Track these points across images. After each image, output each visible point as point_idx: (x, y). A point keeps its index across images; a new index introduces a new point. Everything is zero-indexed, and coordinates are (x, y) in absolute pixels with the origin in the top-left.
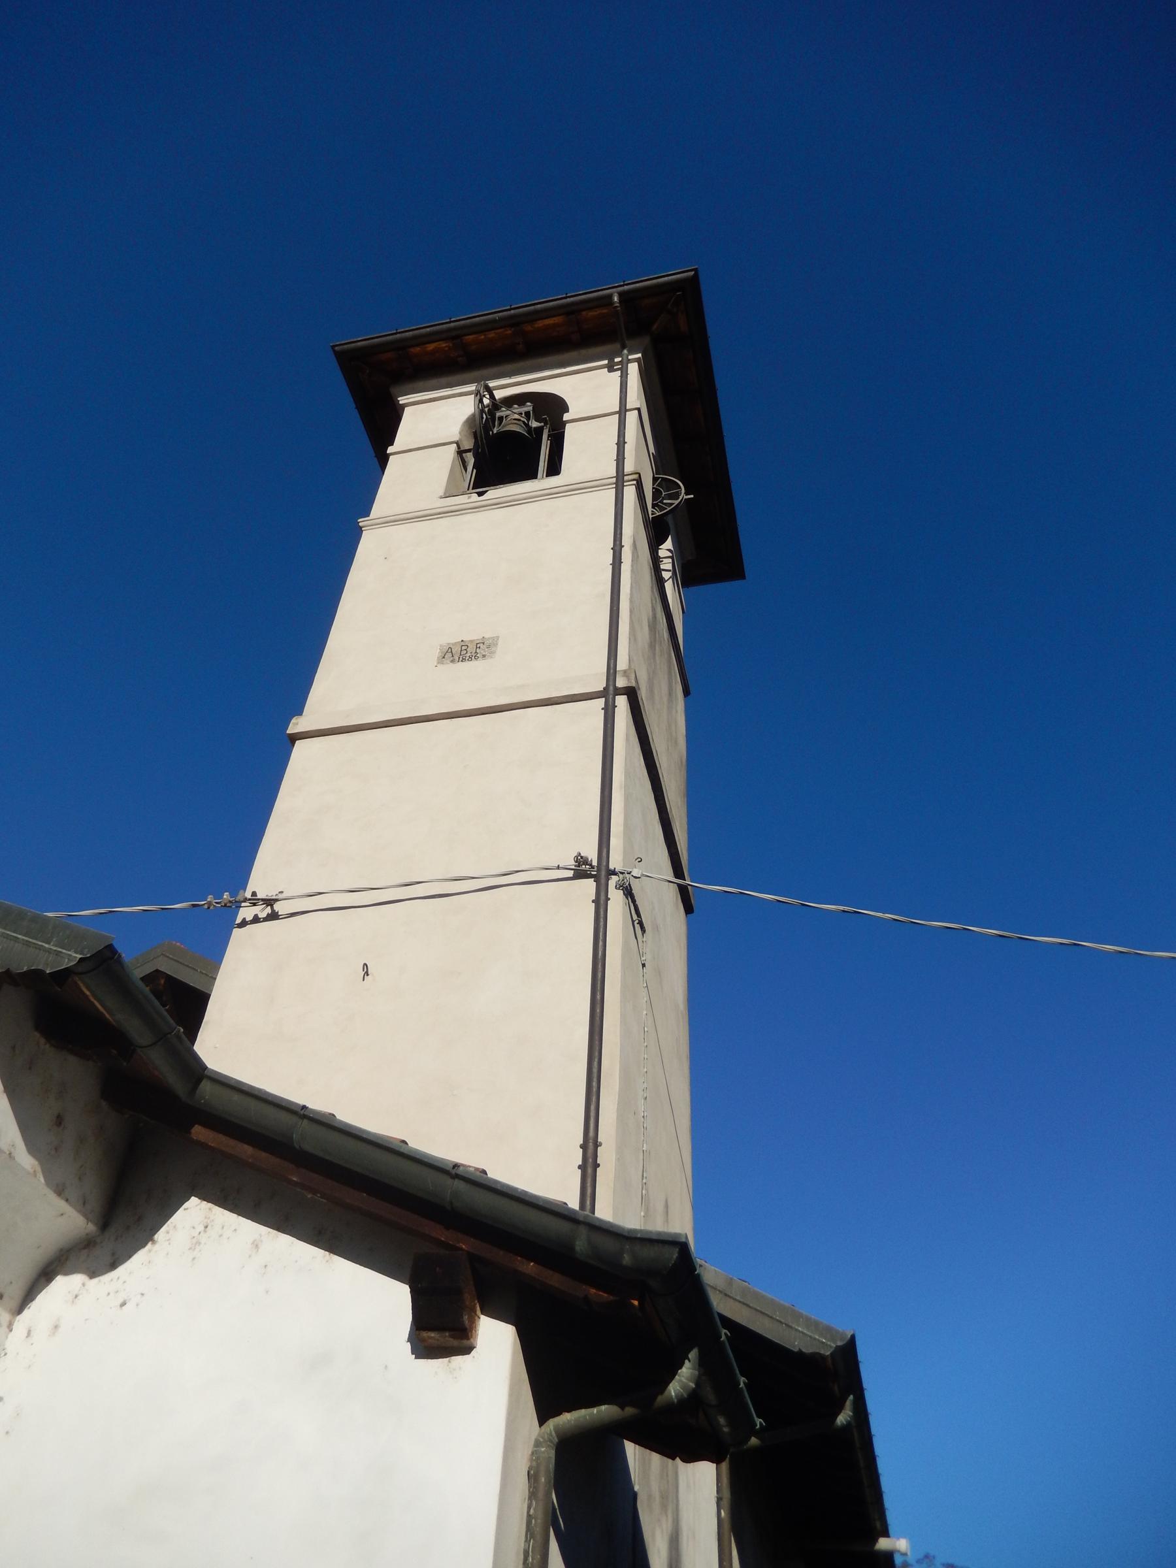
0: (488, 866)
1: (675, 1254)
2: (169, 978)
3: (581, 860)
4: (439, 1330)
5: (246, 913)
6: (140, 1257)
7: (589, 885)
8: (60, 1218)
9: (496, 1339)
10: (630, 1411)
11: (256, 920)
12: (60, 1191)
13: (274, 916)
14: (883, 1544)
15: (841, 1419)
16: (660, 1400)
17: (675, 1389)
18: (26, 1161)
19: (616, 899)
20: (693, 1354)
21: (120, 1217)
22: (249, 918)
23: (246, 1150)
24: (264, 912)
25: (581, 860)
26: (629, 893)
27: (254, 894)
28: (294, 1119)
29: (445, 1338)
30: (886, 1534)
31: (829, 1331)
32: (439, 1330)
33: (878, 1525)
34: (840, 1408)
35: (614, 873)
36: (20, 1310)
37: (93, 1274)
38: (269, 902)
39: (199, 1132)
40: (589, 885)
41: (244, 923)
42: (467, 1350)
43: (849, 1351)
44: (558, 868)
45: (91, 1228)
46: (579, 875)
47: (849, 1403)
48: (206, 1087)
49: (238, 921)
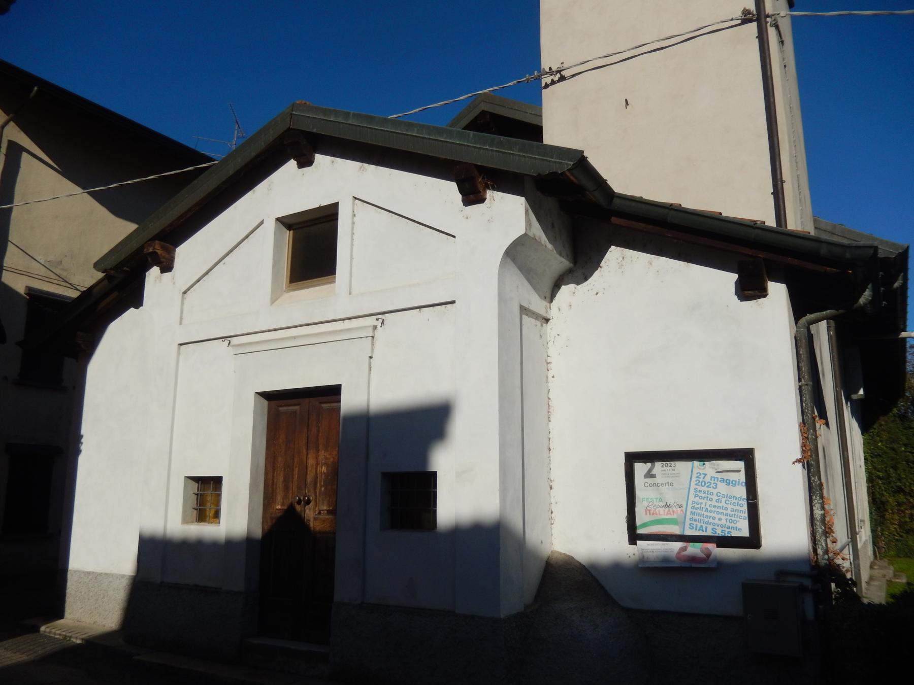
0: (688, 27)
1: (872, 251)
2: (492, 114)
3: (746, 12)
4: (750, 288)
5: (546, 80)
6: (597, 274)
7: (753, 26)
8: (560, 263)
9: (778, 291)
10: (841, 311)
11: (553, 82)
12: (561, 255)
13: (562, 79)
14: (903, 334)
15: (896, 285)
16: (855, 306)
17: (862, 301)
18: (550, 246)
19: (772, 32)
20: (870, 286)
21: (582, 261)
22: (549, 82)
23: (642, 226)
24: (556, 78)
25: (746, 12)
26: (777, 27)
27: (550, 69)
28: (666, 211)
29: (757, 293)
30: (905, 330)
31: (894, 245)
32: (750, 288)
33: (902, 326)
34: (896, 280)
35: (768, 16)
36: (551, 301)
37: (578, 283)
38: (559, 72)
39: (614, 220)
40: (753, 26)
41: (547, 86)
42: (765, 296)
43: (904, 256)
44: (732, 19)
45: (572, 265)
46: (745, 21)
47: (900, 277)
48: (616, 201)
49: (543, 85)
